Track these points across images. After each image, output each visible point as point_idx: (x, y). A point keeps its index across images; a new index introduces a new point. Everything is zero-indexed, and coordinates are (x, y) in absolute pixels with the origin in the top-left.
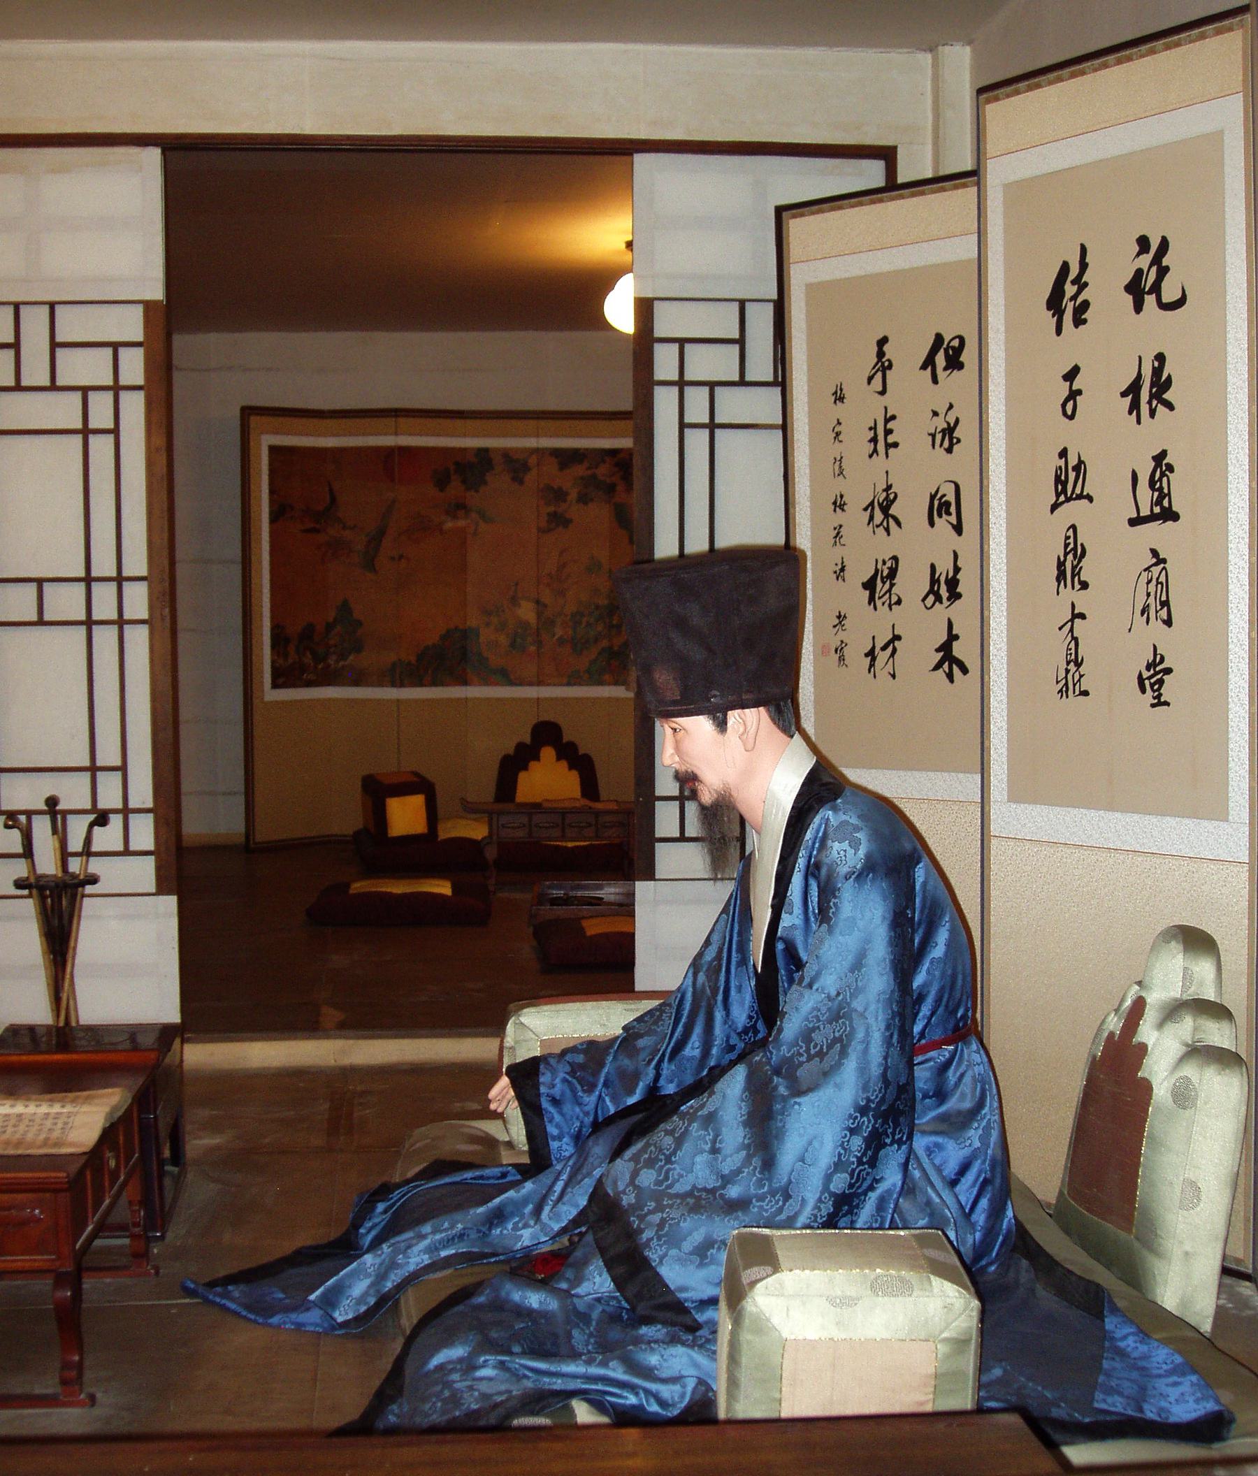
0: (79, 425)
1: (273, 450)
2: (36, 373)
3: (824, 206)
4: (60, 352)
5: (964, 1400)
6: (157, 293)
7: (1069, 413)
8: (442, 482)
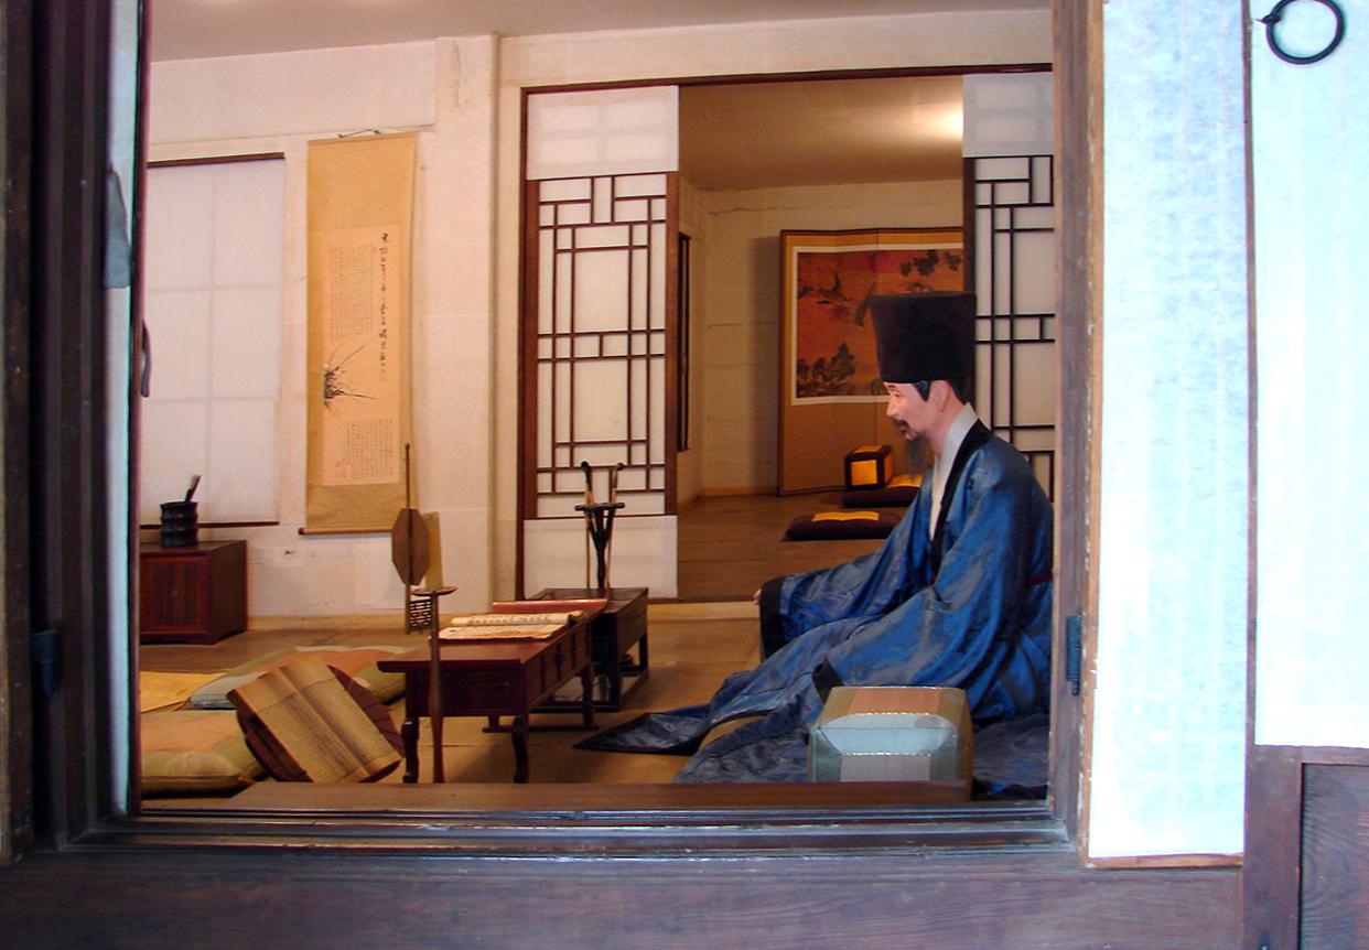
1: (800, 254)
2: (603, 215)
6: (674, 167)
7: (684, 242)
8: (905, 270)
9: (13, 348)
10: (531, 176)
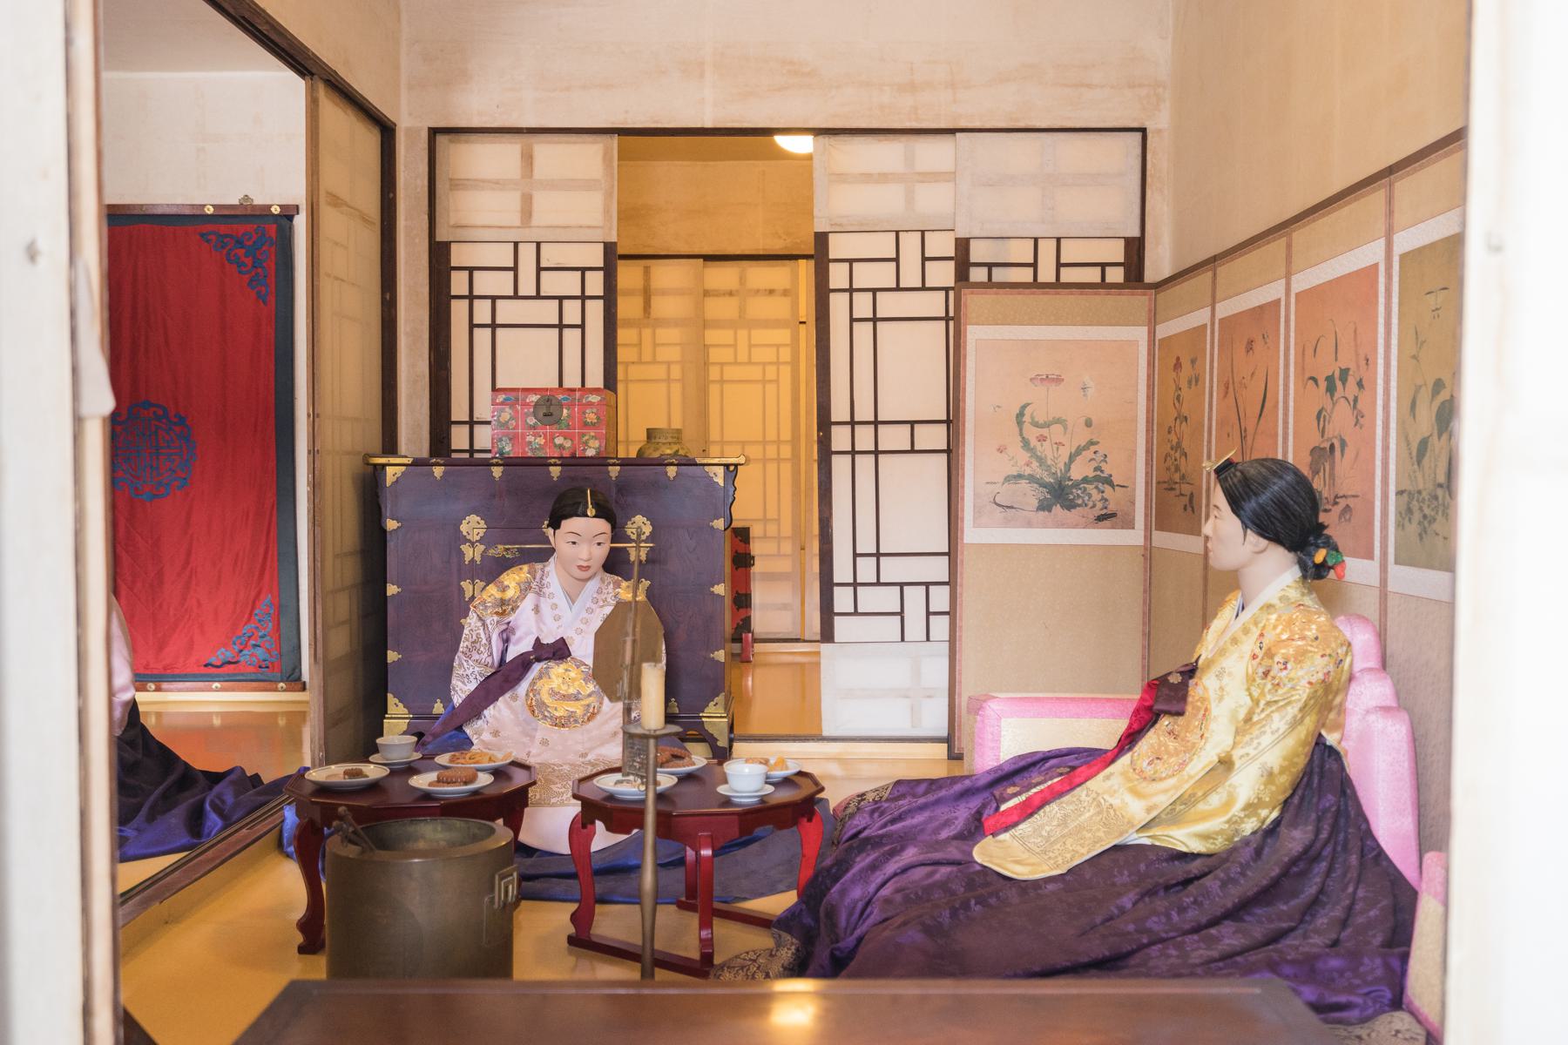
0: (556, 322)
2: (527, 287)
3: (263, 28)
5: (1406, 717)
9: (672, 471)
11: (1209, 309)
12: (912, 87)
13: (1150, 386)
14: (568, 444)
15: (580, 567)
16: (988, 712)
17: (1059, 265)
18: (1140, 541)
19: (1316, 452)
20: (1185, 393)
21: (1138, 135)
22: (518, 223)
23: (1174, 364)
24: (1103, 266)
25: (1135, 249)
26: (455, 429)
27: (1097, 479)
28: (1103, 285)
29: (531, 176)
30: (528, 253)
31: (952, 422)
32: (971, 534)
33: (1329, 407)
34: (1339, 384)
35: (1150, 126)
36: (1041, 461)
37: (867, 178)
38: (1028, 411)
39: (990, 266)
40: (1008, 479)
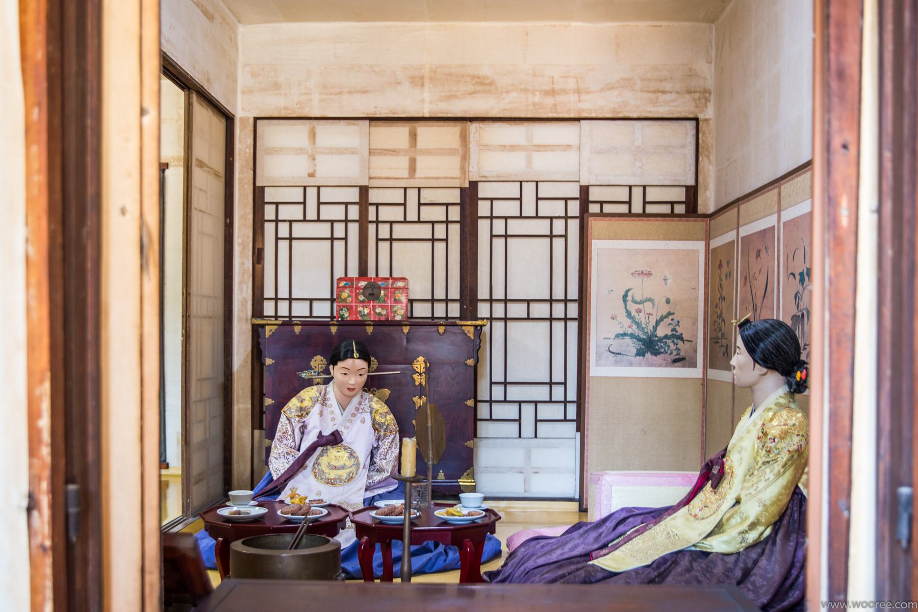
0: (288, 236)
2: (312, 215)
4: (322, 207)
10: (258, 184)
11: (735, 231)
12: (553, 92)
13: (706, 278)
14: (384, 312)
15: (349, 389)
16: (604, 482)
17: (645, 203)
18: (701, 376)
19: (794, 318)
20: (724, 283)
21: (694, 123)
22: (407, 176)
23: (718, 264)
24: (672, 203)
25: (692, 193)
26: (480, 305)
27: (673, 336)
28: (672, 215)
29: (415, 147)
30: (412, 195)
31: (583, 300)
32: (594, 370)
33: (801, 290)
34: (806, 277)
35: (701, 116)
36: (638, 325)
37: (503, 148)
38: (630, 294)
39: (602, 203)
40: (617, 336)
